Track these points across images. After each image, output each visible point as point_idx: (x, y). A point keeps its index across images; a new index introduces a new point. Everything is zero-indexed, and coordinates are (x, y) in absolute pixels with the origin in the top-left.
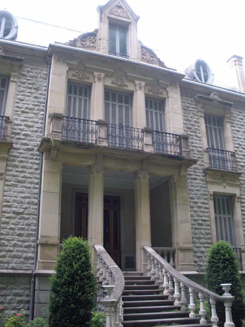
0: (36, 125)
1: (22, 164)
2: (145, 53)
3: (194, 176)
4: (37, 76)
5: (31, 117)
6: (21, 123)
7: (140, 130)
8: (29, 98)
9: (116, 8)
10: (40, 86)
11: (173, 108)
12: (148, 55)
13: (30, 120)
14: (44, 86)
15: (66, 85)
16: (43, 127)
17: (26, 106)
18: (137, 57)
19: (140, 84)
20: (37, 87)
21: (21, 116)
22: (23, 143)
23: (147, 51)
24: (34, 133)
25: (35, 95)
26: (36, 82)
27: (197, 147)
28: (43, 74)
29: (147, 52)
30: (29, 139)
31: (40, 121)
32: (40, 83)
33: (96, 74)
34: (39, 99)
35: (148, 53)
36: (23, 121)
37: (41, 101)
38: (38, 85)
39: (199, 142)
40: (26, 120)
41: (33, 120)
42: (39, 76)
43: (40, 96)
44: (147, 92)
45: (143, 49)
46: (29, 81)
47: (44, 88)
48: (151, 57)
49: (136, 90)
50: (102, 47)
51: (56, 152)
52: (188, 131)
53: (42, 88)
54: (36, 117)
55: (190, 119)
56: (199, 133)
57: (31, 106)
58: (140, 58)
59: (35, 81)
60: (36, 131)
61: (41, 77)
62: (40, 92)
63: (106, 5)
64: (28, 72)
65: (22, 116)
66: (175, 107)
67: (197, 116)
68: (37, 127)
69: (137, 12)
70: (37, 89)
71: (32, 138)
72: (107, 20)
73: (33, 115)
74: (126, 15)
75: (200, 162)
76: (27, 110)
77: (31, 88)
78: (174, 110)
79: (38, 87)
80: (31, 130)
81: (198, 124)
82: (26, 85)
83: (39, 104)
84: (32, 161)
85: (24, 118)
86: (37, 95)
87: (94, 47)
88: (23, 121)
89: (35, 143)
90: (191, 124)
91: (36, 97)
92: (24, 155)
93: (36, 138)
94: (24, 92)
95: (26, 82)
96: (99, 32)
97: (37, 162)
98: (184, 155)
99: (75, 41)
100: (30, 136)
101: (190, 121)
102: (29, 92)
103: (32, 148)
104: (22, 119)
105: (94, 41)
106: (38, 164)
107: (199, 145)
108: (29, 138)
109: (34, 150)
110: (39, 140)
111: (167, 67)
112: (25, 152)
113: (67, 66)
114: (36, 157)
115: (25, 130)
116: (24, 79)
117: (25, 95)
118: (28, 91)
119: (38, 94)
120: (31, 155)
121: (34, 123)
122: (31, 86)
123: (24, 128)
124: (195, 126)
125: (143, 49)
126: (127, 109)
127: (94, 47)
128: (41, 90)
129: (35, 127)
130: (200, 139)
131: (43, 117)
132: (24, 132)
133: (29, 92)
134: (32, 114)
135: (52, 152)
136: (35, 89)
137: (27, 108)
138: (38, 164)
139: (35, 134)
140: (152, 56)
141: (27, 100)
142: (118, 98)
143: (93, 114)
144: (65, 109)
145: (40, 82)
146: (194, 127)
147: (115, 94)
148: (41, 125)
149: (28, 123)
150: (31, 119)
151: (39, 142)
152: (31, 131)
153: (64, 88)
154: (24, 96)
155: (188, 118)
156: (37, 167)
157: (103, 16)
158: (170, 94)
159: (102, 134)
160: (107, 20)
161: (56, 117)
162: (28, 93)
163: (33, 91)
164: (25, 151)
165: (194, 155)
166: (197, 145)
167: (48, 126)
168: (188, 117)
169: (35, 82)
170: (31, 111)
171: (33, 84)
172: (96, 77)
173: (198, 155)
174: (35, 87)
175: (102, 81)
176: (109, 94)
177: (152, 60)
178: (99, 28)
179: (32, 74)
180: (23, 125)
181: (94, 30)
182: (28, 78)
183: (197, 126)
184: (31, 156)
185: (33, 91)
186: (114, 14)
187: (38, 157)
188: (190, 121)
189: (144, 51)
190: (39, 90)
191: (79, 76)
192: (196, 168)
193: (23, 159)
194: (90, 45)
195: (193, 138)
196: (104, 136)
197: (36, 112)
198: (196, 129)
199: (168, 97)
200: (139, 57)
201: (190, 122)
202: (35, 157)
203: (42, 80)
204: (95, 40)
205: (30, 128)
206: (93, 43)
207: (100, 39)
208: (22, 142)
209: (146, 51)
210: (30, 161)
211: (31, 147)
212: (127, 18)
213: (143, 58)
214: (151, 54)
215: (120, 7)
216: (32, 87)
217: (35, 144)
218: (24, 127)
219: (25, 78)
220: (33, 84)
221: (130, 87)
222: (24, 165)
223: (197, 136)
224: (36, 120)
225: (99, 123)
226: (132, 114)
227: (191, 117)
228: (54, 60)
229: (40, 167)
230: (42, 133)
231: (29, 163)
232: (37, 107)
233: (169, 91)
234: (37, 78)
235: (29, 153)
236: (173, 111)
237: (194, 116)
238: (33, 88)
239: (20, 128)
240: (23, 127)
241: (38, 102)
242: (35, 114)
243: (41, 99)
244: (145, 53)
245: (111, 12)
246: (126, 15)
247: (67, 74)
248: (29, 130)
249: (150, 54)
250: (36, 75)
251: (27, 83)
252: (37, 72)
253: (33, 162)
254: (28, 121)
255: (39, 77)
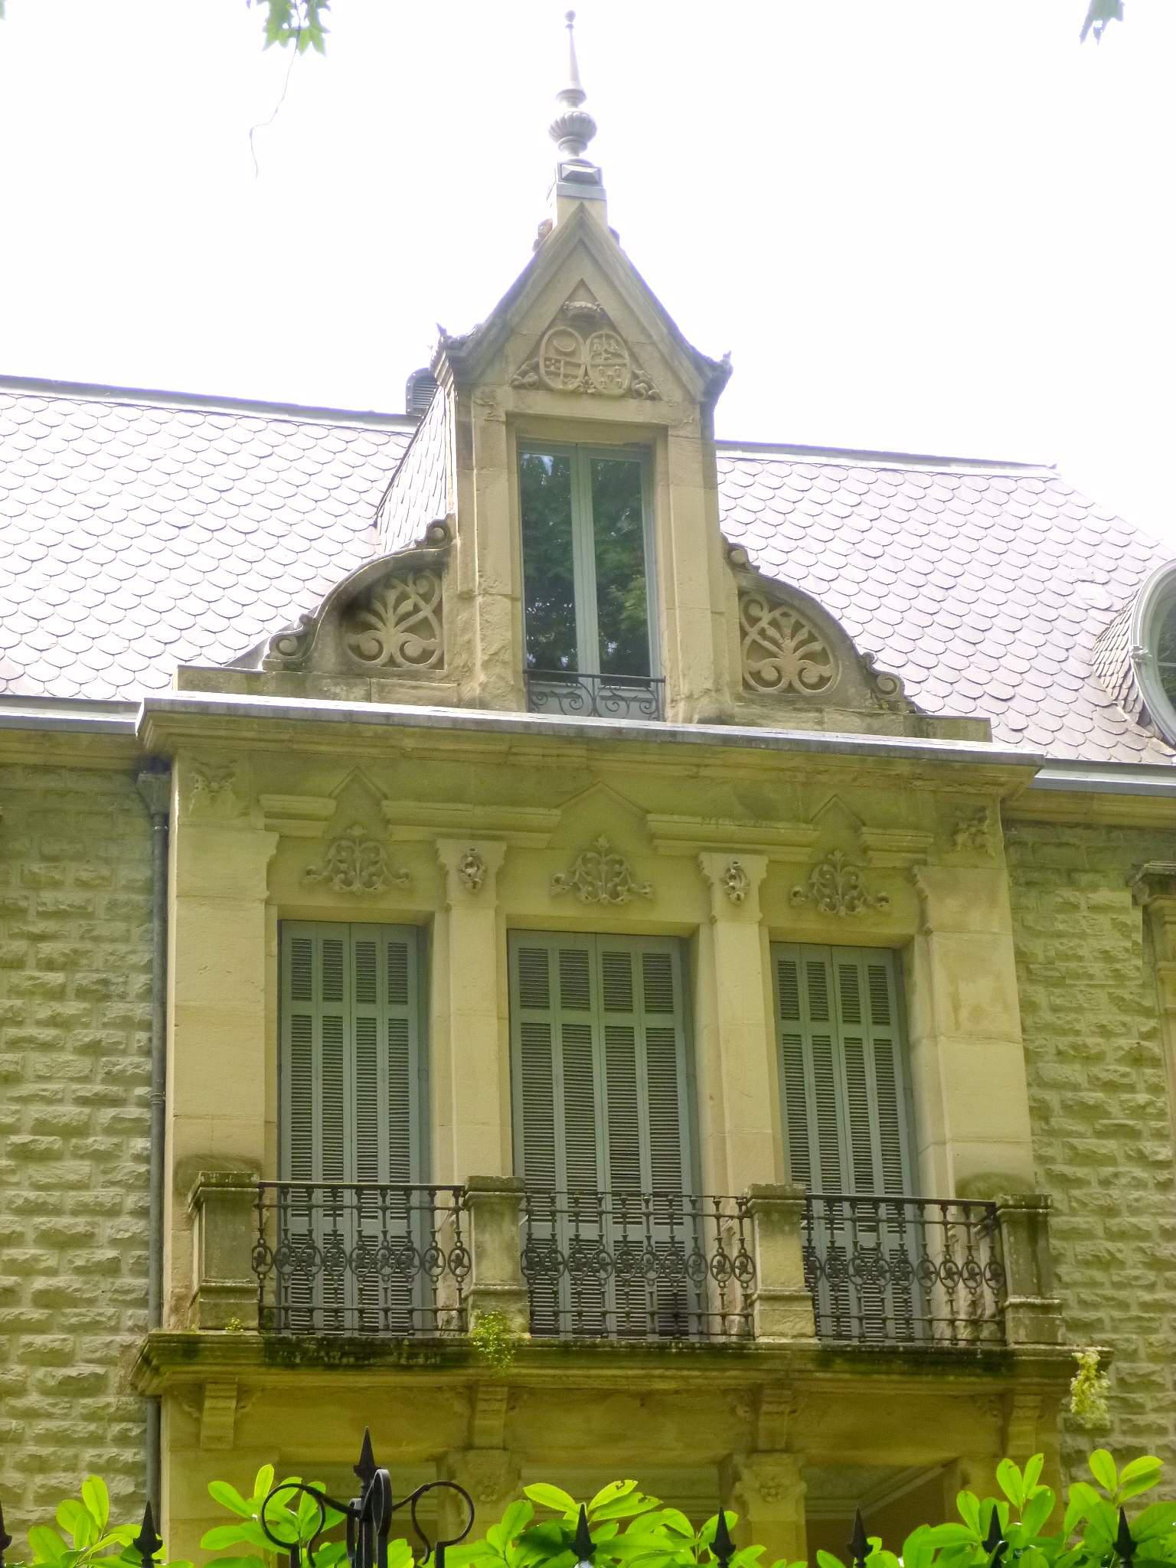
0: (107, 1229)
1: (39, 1479)
2: (772, 632)
3: (1124, 1433)
4: (88, 901)
5: (77, 1177)
6: (19, 1229)
7: (731, 1208)
8: (54, 1056)
9: (563, 333)
10: (114, 968)
11: (956, 1008)
12: (789, 644)
13: (72, 1198)
14: (134, 967)
15: (268, 955)
16: (150, 1236)
17: (36, 1111)
18: (709, 685)
19: (733, 877)
20: (96, 976)
21: (14, 1179)
22: (36, 1352)
23: (784, 615)
24: (97, 1278)
25: (87, 1036)
26: (88, 945)
27: (1145, 1236)
28: (126, 888)
29: (783, 621)
30: (73, 1320)
31: (131, 1201)
32: (108, 947)
33: (450, 854)
34: (113, 1059)
35: (788, 631)
36: (30, 1209)
37: (124, 1071)
38: (99, 963)
39: (1157, 1197)
40: (44, 1203)
41: (87, 1196)
42: (102, 899)
43: (118, 1035)
44: (784, 920)
45: (755, 611)
46: (46, 949)
47: (139, 981)
48: (810, 656)
49: (712, 921)
50: (480, 657)
51: (233, 1404)
52: (1081, 1135)
53: (125, 983)
54: (102, 1178)
55: (1094, 1042)
56: (1160, 1135)
57: (69, 1112)
58: (732, 684)
59: (82, 938)
60: (112, 1268)
61: (112, 905)
62: (116, 1009)
63: (492, 324)
64: (34, 884)
65: (17, 1184)
66: (977, 991)
67: (1148, 1013)
68: (114, 1242)
69: (704, 337)
70: (99, 994)
71: (89, 1314)
72: (503, 445)
73: (85, 1167)
74: (635, 376)
75: (1161, 1336)
76: (45, 1141)
77: (57, 994)
78: (964, 1014)
79: (98, 982)
80: (79, 1263)
81: (1149, 1071)
82: (28, 973)
83: (115, 1089)
84: (100, 1456)
85: (32, 1195)
86: (101, 1034)
87: (433, 659)
88: (30, 1209)
89: (109, 1339)
90: (1104, 1076)
91: (94, 1049)
92: (52, 1425)
93: (111, 1311)
94: (20, 1024)
95: (26, 954)
96: (458, 541)
97: (129, 1455)
98: (1019, 1337)
99: (305, 637)
100: (74, 1302)
101: (1099, 1057)
102: (53, 1022)
103: (96, 1376)
104: (20, 1202)
105: (426, 611)
106: (130, 1469)
107: (1162, 1221)
108: (72, 1315)
109: (106, 1386)
110: (130, 1323)
111: (928, 701)
112: (54, 1405)
113: (267, 828)
114: (124, 1425)
115: (43, 1265)
116: (13, 936)
117: (24, 1040)
118: (44, 1014)
119: (105, 1025)
120: (91, 1417)
121: (98, 1219)
122: (56, 978)
123: (36, 1259)
124: (1131, 1088)
125: (755, 611)
126: (662, 1043)
127: (433, 659)
128: (122, 997)
129: (104, 1240)
130: (1163, 1175)
131: (148, 1171)
132: (40, 1283)
133: (53, 1022)
134: (78, 1162)
135: (207, 1404)
136: (82, 993)
137: (42, 1127)
138: (130, 1469)
139: (106, 1283)
140: (816, 646)
141: (44, 1072)
142: (596, 995)
143: (446, 1124)
144: (274, 1118)
145: (113, 940)
146: (1125, 1096)
147: (582, 956)
148: (137, 1226)
149: (62, 1222)
150: (72, 1193)
151: (129, 888)
152: (79, 1271)
153: (261, 979)
154: (24, 1049)
155: (1079, 1040)
156: (131, 1489)
157: (477, 419)
158: (943, 910)
159: (496, 1267)
160: (502, 444)
161: (220, 1193)
162: (39, 1023)
163: (72, 1007)
164: (51, 1401)
165: (1122, 1294)
166: (1145, 1221)
167: (175, 1238)
168: (1077, 1033)
169: (78, 946)
170: (74, 1141)
171: (69, 964)
172: (453, 879)
173: (1151, 1287)
174: (83, 978)
175: (490, 894)
176: (537, 971)
177: (814, 680)
178: (455, 510)
179: (60, 895)
180: (31, 1235)
181: (421, 534)
182: (39, 927)
183: (1141, 1086)
184: (92, 1427)
185: (72, 1007)
186: (549, 389)
187: (130, 1425)
188: (1099, 1057)
189: (759, 619)
190: (107, 997)
191: (348, 882)
192: (1133, 1380)
193: (45, 1451)
194: (402, 649)
195: (1116, 1175)
196: (515, 1279)
197: (99, 1142)
198: (1139, 1111)
199: (928, 933)
200: (727, 678)
201: (1096, 1070)
202: (116, 1428)
203: (120, 927)
204: (435, 600)
205: (71, 1253)
206: (423, 628)
207: (467, 597)
208: (30, 1345)
209: (774, 623)
210: (89, 1454)
211: (87, 1369)
212: (638, 394)
213: (757, 676)
214: (812, 638)
215: (589, 322)
216: (63, 986)
217: (108, 1345)
218: (39, 1252)
219: (16, 926)
220: (69, 964)
221: (670, 909)
222: (53, 1482)
223: (1141, 1158)
224: (106, 1195)
225: (475, 1196)
226: (692, 1078)
227: (1104, 1031)
228: (184, 798)
229: (149, 1484)
230: (146, 1274)
231: (83, 1464)
232: (107, 1114)
233: (928, 892)
234: (89, 916)
235: (78, 1410)
236: (957, 1023)
237: (1127, 1019)
238: (70, 991)
239: (13, 1261)
240: (34, 1251)
241: (110, 1078)
242: (98, 1156)
243: (124, 1053)
244: (772, 632)
245: (532, 378)
246: (635, 376)
247: (277, 848)
248: (71, 1262)
249: (803, 635)
250: (78, 897)
251: (31, 961)
252: (84, 876)
253: (105, 1457)
254: (57, 1211)
255: (101, 913)
